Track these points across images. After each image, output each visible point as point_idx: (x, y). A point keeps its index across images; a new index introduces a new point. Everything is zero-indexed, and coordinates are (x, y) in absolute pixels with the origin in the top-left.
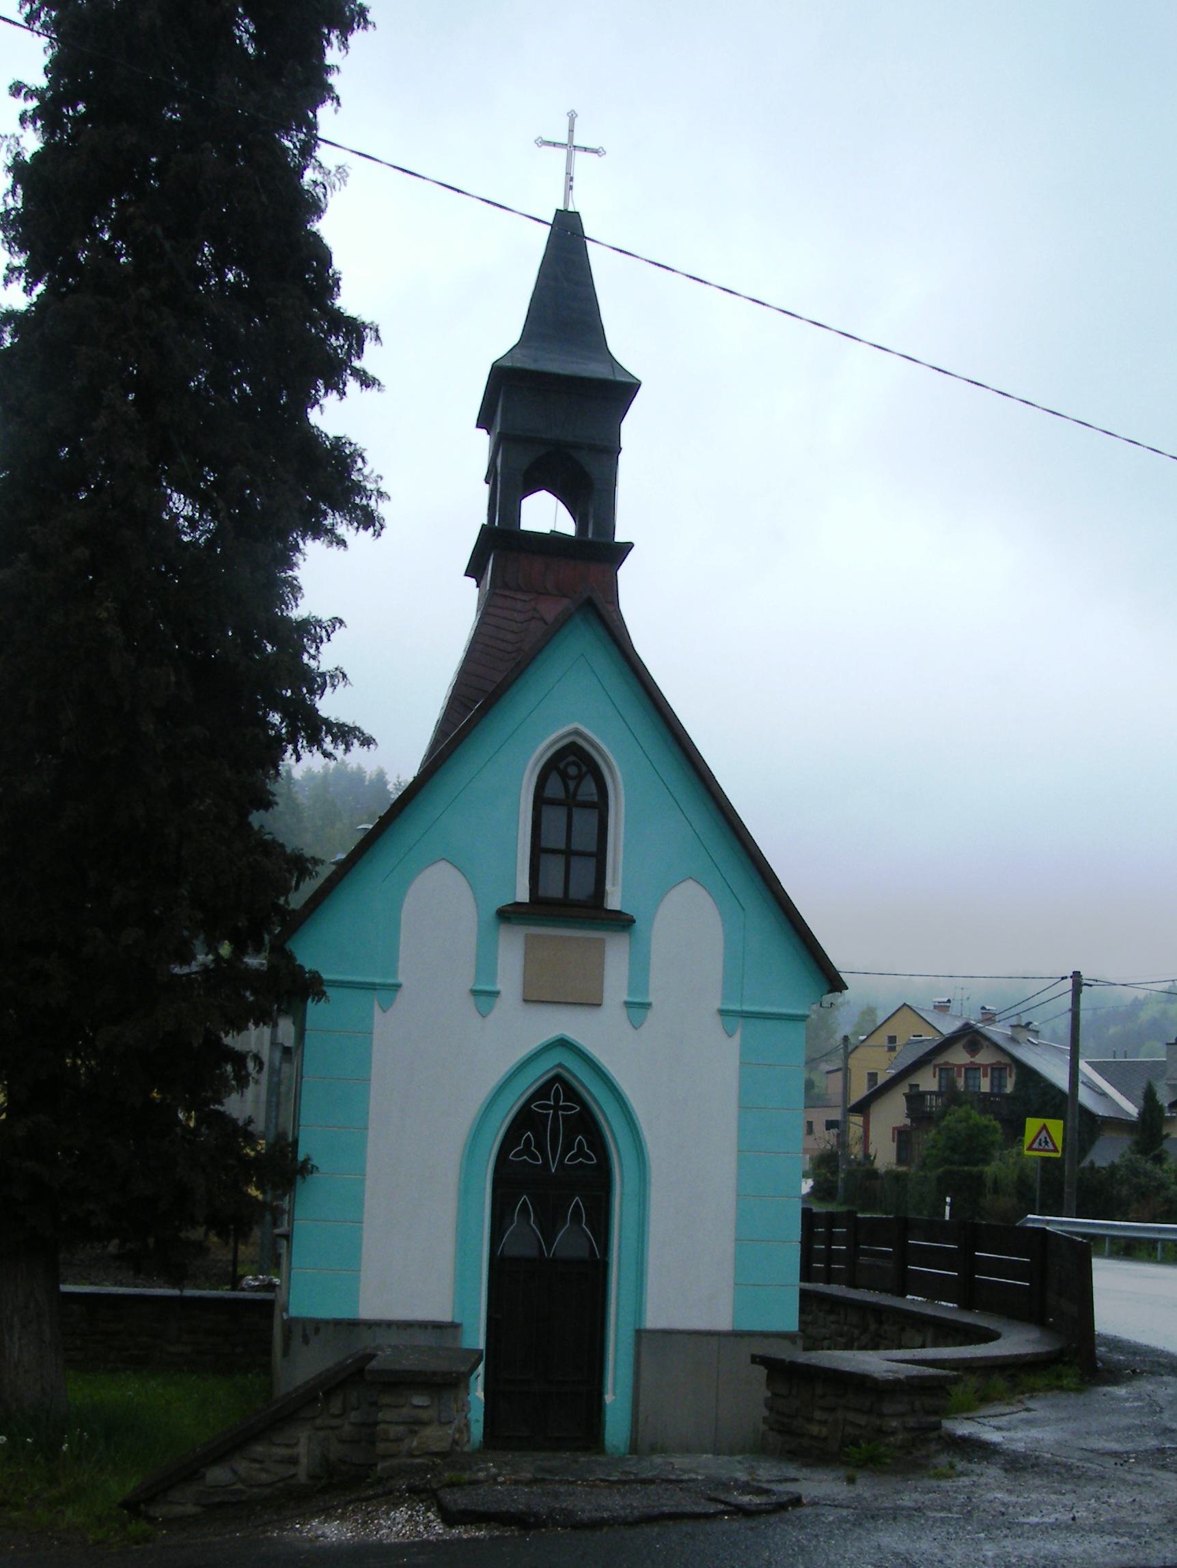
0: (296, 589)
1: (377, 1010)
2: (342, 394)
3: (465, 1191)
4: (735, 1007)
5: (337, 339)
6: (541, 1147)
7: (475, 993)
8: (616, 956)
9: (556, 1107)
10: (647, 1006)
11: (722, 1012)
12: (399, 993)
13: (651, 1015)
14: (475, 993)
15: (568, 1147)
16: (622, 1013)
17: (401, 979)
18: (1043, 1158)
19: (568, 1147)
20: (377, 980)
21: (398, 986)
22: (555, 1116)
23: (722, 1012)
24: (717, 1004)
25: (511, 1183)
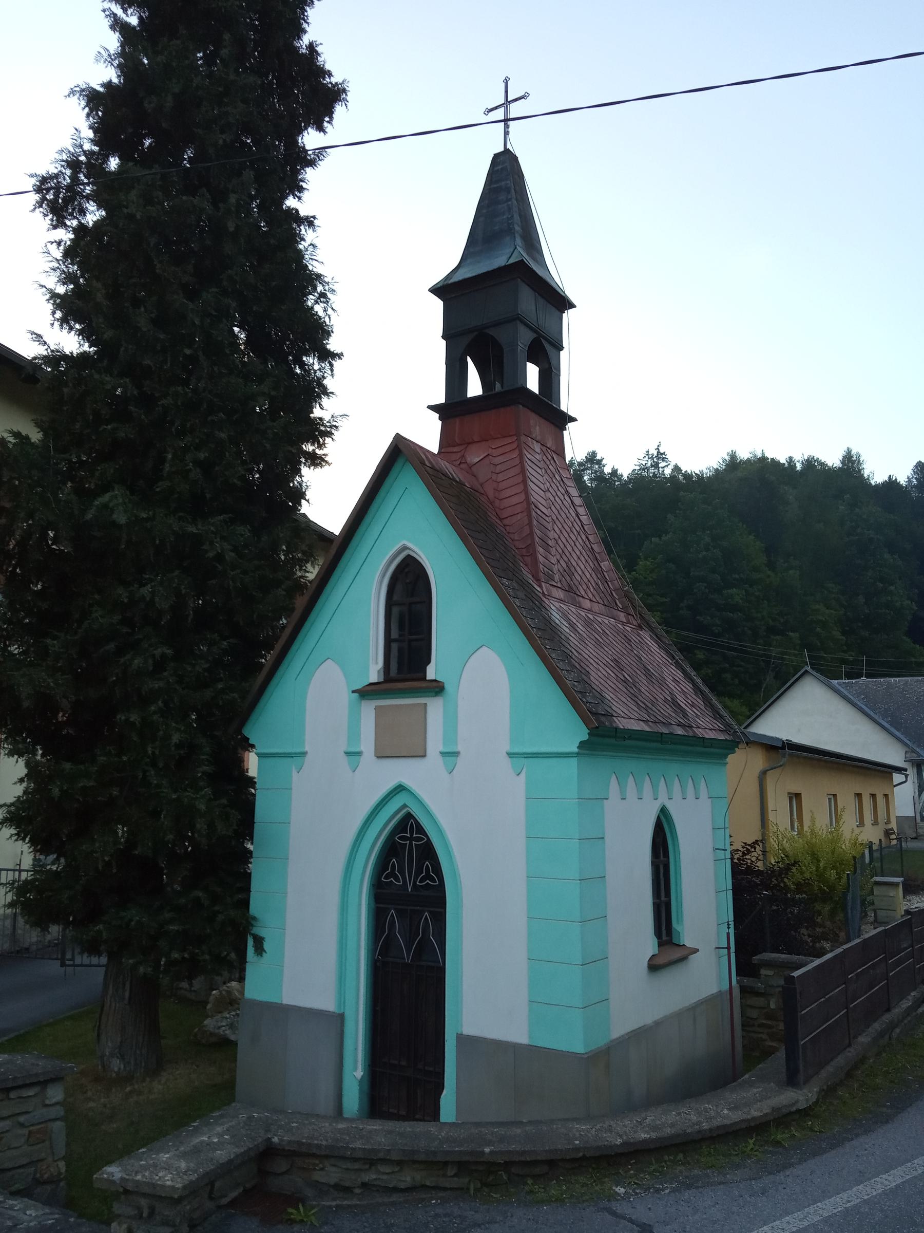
0: (701, 472)
1: (294, 773)
2: (310, 222)
3: (455, 875)
4: (516, 750)
5: (224, 141)
6: (402, 872)
7: (348, 754)
8: (435, 708)
9: (411, 839)
10: (456, 754)
11: (511, 755)
12: (306, 759)
13: (460, 761)
14: (348, 754)
15: (419, 872)
16: (440, 760)
17: (307, 748)
18: (738, 974)
19: (419, 872)
20: (293, 751)
21: (305, 754)
22: (411, 844)
23: (511, 755)
24: (506, 746)
25: (384, 895)
